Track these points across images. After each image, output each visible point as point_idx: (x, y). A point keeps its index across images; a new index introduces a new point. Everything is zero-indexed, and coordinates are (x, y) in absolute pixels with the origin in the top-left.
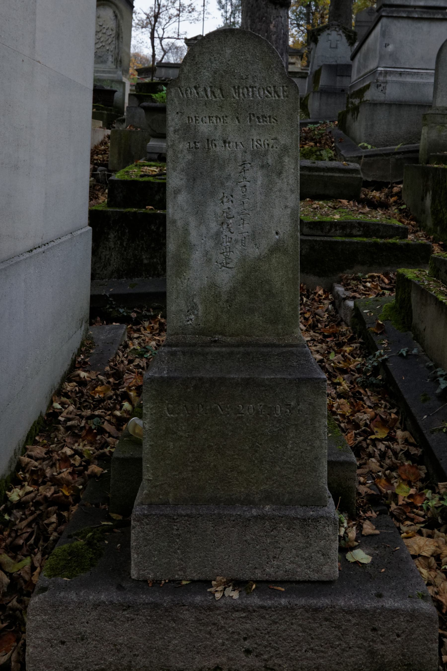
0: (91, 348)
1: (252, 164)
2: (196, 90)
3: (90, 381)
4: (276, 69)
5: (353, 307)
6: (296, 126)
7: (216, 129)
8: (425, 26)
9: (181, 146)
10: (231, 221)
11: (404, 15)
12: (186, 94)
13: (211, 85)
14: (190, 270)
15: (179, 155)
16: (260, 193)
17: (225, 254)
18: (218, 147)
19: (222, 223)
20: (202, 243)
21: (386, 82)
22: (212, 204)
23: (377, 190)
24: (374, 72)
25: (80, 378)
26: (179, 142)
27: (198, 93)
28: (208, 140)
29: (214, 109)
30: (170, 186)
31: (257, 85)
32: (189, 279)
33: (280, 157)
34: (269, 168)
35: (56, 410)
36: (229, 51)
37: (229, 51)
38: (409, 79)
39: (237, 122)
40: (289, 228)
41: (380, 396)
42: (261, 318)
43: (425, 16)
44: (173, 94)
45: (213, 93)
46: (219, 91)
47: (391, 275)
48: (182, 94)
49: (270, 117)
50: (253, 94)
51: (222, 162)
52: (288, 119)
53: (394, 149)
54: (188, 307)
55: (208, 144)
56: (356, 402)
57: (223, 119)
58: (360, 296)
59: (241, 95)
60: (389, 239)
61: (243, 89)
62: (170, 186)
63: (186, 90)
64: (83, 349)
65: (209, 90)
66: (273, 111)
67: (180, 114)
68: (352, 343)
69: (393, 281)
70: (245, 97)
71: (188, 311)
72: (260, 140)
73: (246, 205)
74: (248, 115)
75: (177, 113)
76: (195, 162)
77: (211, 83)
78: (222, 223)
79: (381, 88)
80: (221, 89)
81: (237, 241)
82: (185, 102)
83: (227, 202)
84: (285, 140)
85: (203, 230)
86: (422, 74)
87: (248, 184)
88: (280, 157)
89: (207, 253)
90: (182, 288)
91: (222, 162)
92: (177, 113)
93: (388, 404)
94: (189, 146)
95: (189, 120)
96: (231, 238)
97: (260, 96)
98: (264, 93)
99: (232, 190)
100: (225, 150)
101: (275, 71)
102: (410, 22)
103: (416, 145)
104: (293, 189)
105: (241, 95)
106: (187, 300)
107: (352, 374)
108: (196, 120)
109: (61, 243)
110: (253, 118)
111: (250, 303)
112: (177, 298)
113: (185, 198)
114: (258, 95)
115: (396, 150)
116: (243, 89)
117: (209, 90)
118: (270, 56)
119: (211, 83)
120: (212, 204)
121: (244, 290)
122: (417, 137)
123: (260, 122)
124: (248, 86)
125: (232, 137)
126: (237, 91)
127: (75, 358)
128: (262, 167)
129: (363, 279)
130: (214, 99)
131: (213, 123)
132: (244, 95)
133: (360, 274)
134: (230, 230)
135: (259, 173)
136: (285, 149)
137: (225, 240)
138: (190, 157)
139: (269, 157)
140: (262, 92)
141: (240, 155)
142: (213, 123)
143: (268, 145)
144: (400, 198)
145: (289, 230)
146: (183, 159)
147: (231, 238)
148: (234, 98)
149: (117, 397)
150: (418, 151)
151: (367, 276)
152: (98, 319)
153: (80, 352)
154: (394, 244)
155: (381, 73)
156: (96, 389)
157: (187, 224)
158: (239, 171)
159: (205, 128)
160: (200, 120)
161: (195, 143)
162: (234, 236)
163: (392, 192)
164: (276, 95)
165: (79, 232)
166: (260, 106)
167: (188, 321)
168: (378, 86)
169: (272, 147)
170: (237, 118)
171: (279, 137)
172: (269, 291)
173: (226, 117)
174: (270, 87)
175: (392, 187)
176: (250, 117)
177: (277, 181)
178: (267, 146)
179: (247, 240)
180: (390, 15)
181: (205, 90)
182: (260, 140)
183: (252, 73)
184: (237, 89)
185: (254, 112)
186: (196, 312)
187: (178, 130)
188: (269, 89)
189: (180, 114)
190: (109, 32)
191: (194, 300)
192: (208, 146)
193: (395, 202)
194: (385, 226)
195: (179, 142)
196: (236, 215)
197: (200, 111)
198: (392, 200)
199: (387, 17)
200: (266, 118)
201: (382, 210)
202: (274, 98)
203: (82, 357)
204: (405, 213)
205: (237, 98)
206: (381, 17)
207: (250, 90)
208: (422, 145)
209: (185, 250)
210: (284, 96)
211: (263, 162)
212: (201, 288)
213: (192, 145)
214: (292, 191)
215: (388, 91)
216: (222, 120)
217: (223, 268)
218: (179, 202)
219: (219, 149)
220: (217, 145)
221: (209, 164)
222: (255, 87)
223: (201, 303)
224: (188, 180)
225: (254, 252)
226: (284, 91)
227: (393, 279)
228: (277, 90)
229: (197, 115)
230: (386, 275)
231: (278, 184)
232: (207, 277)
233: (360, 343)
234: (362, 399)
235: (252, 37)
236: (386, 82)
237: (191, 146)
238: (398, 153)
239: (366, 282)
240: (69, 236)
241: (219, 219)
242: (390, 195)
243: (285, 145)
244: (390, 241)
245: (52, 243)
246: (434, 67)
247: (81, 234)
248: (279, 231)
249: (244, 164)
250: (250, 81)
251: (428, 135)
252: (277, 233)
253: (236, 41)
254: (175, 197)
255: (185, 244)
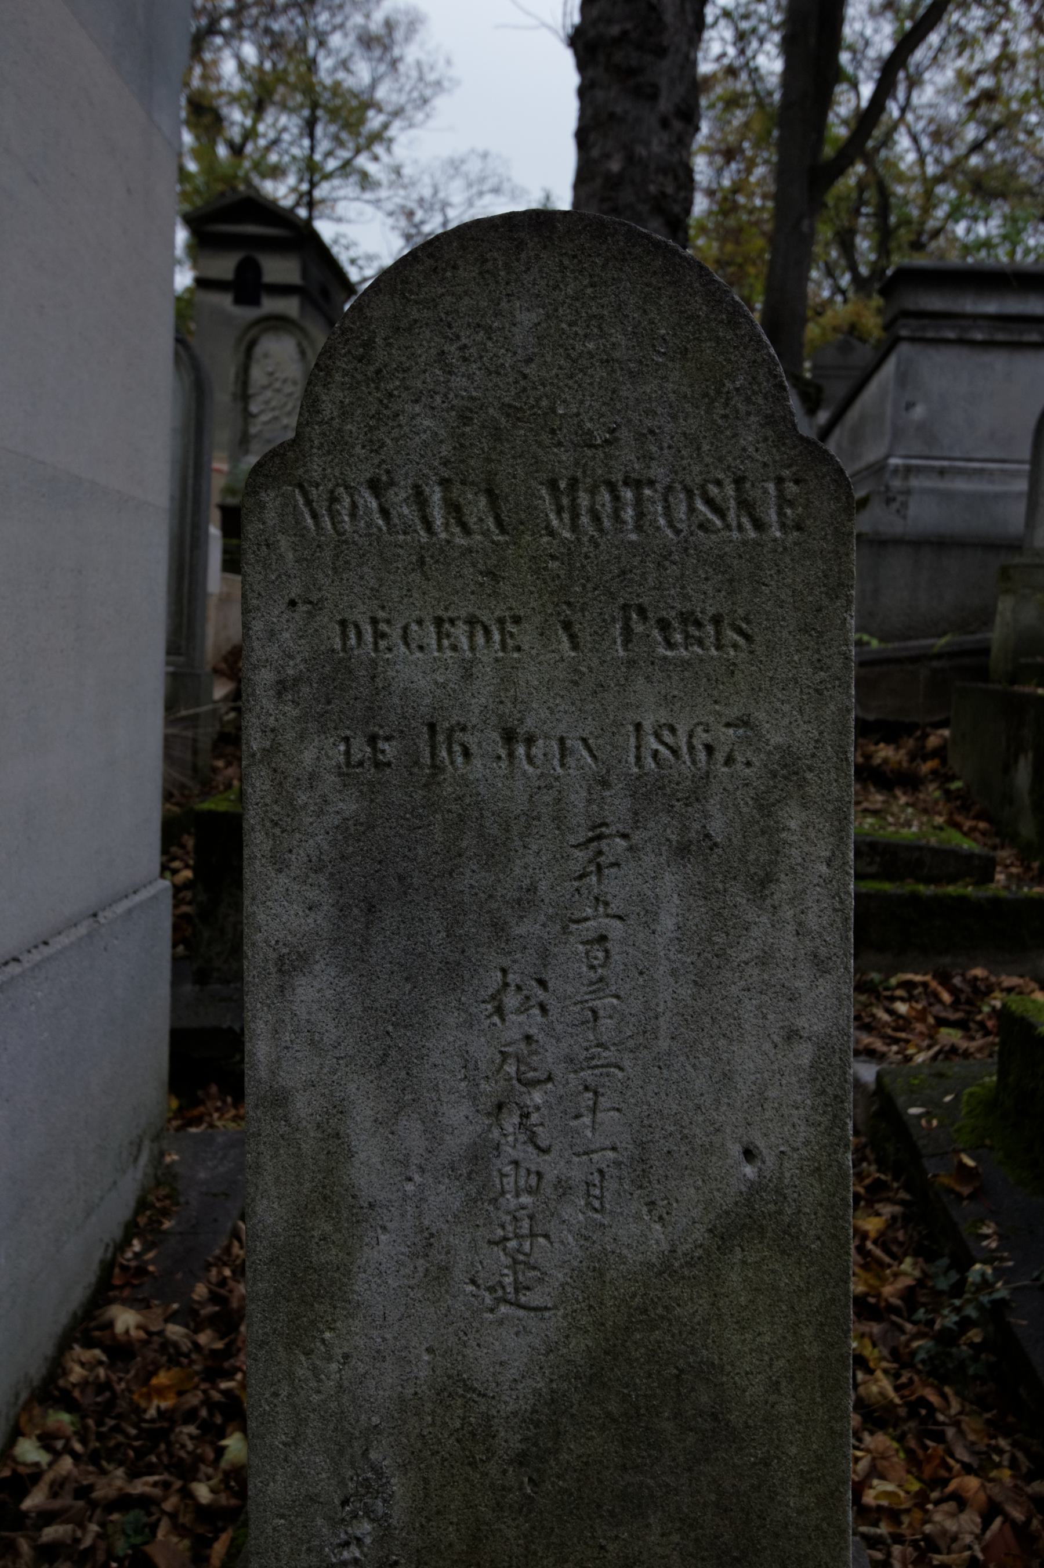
0: (165, 1213)
1: (637, 837)
2: (377, 497)
3: (146, 1343)
4: (748, 400)
5: (872, 1087)
6: (838, 664)
7: (468, 675)
8: (999, 361)
9: (308, 756)
10: (537, 1096)
11: (951, 335)
12: (333, 515)
13: (446, 474)
14: (351, 1316)
15: (302, 798)
16: (674, 973)
17: (512, 1244)
18: (477, 762)
19: (500, 1106)
20: (405, 1198)
21: (908, 492)
22: (451, 1021)
23: (888, 742)
24: (878, 469)
25: (114, 1336)
26: (302, 737)
27: (385, 513)
28: (432, 727)
29: (459, 584)
30: (258, 937)
31: (658, 472)
32: (346, 1356)
33: (765, 807)
34: (714, 859)
35: (21, 1469)
36: (527, 318)
37: (527, 318)
38: (961, 485)
39: (566, 644)
40: (804, 1131)
41: (988, 1415)
42: (676, 1538)
43: (1000, 337)
44: (271, 517)
45: (454, 509)
46: (483, 501)
47: (957, 981)
48: (315, 516)
49: (717, 620)
50: (640, 515)
51: (495, 830)
52: (805, 629)
53: (932, 646)
54: (342, 1483)
55: (433, 748)
56: (926, 1448)
57: (502, 631)
58: (885, 1049)
59: (585, 519)
60: (949, 883)
61: (593, 491)
62: (258, 937)
63: (333, 499)
64: (142, 1221)
65: (436, 496)
66: (732, 593)
67: (303, 608)
68: (879, 1201)
69: (963, 997)
70: (601, 531)
71: (345, 1502)
72: (673, 730)
73: (606, 1023)
74: (618, 614)
75: (292, 603)
76: (372, 827)
77: (446, 463)
78: (500, 1106)
79: (895, 506)
80: (490, 493)
81: (563, 1187)
82: (327, 555)
83: (519, 1012)
84: (785, 727)
85: (412, 1134)
86: (991, 472)
87: (615, 929)
88: (765, 807)
89: (430, 1239)
90: (315, 1398)
91: (495, 830)
92: (292, 603)
93: (1020, 1455)
94: (347, 753)
95: (345, 637)
96: (539, 1175)
97: (671, 524)
98: (692, 510)
99: (544, 955)
100: (511, 776)
101: (742, 408)
102: (965, 352)
103: (979, 636)
104: (823, 951)
105: (585, 519)
106: (341, 1452)
107: (894, 1324)
108: (379, 635)
109: (48, 959)
110: (639, 628)
111: (624, 1468)
112: (295, 1442)
113: (329, 993)
114: (662, 521)
115: (935, 650)
116: (593, 491)
117: (436, 496)
118: (718, 340)
119: (446, 463)
120: (451, 1021)
121: (596, 1411)
122: (986, 617)
123: (670, 645)
124: (618, 477)
125: (544, 714)
126: (565, 501)
127: (114, 1255)
128: (683, 850)
129: (887, 989)
130: (460, 541)
131: (454, 648)
132: (596, 518)
133: (875, 976)
134: (532, 1139)
135: (667, 876)
136: (788, 769)
137: (509, 1183)
138: (349, 806)
139: (713, 806)
140: (683, 508)
141: (577, 798)
142: (454, 648)
143: (709, 749)
144: (944, 761)
145: (807, 1143)
146: (320, 813)
147: (539, 1175)
148: (551, 533)
149: (211, 1414)
150: (986, 651)
151: (893, 981)
152: (214, 1089)
153: (131, 1229)
154: (962, 899)
155: (896, 470)
156: (154, 1381)
157: (340, 1109)
158: (577, 868)
159: (417, 671)
160: (395, 634)
161: (372, 740)
162: (553, 1167)
163: (923, 747)
164: (745, 520)
165: (121, 908)
166: (673, 570)
167: (346, 1544)
168: (889, 501)
169: (729, 761)
170: (567, 626)
171: (761, 715)
172: (714, 1416)
173: (517, 620)
174: (719, 483)
175: (925, 736)
176: (627, 620)
177: (750, 917)
178: (702, 756)
179: (611, 1185)
180: (918, 334)
181: (420, 499)
182: (673, 730)
183: (635, 417)
184: (564, 491)
185: (645, 600)
186: (379, 1506)
187: (297, 680)
188: (713, 490)
189: (303, 608)
190: (289, 389)
191: (373, 1455)
192: (433, 755)
193: (934, 772)
194: (935, 852)
195: (302, 737)
196: (558, 1071)
197: (396, 593)
198: (926, 767)
199: (912, 340)
200: (699, 624)
201: (905, 793)
202: (735, 535)
203: (137, 1246)
204: (961, 804)
205: (567, 534)
206: (896, 341)
207: (628, 495)
208: (997, 636)
209: (328, 1228)
210: (783, 526)
211: (685, 829)
212: (401, 1398)
213: (361, 750)
214: (820, 965)
215: (912, 511)
216: (497, 637)
217: (503, 1309)
218: (302, 1013)
219: (483, 768)
220: (474, 749)
221: (439, 837)
222: (651, 483)
223: (404, 1467)
224: (343, 910)
225: (641, 1236)
226: (783, 501)
227: (961, 991)
228: (754, 494)
229: (381, 614)
230: (944, 978)
231: (755, 932)
232: (430, 1350)
233: (902, 1203)
234: (940, 1437)
235: (638, 250)
236: (908, 492)
237: (357, 757)
238: (939, 656)
239: (893, 999)
240: (82, 930)
241: (484, 1086)
242: (920, 754)
243: (786, 751)
244: (951, 889)
245: (13, 964)
246: (1027, 455)
247: (130, 911)
248: (761, 1143)
249: (599, 837)
250: (627, 456)
251: (1011, 617)
252: (749, 1154)
253: (563, 268)
254: (282, 989)
255: (331, 1199)
